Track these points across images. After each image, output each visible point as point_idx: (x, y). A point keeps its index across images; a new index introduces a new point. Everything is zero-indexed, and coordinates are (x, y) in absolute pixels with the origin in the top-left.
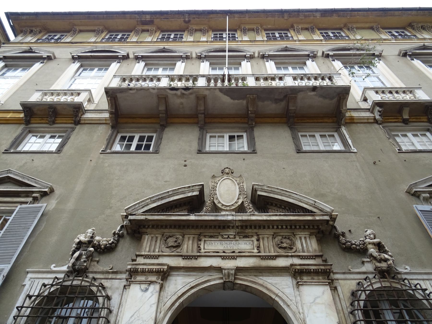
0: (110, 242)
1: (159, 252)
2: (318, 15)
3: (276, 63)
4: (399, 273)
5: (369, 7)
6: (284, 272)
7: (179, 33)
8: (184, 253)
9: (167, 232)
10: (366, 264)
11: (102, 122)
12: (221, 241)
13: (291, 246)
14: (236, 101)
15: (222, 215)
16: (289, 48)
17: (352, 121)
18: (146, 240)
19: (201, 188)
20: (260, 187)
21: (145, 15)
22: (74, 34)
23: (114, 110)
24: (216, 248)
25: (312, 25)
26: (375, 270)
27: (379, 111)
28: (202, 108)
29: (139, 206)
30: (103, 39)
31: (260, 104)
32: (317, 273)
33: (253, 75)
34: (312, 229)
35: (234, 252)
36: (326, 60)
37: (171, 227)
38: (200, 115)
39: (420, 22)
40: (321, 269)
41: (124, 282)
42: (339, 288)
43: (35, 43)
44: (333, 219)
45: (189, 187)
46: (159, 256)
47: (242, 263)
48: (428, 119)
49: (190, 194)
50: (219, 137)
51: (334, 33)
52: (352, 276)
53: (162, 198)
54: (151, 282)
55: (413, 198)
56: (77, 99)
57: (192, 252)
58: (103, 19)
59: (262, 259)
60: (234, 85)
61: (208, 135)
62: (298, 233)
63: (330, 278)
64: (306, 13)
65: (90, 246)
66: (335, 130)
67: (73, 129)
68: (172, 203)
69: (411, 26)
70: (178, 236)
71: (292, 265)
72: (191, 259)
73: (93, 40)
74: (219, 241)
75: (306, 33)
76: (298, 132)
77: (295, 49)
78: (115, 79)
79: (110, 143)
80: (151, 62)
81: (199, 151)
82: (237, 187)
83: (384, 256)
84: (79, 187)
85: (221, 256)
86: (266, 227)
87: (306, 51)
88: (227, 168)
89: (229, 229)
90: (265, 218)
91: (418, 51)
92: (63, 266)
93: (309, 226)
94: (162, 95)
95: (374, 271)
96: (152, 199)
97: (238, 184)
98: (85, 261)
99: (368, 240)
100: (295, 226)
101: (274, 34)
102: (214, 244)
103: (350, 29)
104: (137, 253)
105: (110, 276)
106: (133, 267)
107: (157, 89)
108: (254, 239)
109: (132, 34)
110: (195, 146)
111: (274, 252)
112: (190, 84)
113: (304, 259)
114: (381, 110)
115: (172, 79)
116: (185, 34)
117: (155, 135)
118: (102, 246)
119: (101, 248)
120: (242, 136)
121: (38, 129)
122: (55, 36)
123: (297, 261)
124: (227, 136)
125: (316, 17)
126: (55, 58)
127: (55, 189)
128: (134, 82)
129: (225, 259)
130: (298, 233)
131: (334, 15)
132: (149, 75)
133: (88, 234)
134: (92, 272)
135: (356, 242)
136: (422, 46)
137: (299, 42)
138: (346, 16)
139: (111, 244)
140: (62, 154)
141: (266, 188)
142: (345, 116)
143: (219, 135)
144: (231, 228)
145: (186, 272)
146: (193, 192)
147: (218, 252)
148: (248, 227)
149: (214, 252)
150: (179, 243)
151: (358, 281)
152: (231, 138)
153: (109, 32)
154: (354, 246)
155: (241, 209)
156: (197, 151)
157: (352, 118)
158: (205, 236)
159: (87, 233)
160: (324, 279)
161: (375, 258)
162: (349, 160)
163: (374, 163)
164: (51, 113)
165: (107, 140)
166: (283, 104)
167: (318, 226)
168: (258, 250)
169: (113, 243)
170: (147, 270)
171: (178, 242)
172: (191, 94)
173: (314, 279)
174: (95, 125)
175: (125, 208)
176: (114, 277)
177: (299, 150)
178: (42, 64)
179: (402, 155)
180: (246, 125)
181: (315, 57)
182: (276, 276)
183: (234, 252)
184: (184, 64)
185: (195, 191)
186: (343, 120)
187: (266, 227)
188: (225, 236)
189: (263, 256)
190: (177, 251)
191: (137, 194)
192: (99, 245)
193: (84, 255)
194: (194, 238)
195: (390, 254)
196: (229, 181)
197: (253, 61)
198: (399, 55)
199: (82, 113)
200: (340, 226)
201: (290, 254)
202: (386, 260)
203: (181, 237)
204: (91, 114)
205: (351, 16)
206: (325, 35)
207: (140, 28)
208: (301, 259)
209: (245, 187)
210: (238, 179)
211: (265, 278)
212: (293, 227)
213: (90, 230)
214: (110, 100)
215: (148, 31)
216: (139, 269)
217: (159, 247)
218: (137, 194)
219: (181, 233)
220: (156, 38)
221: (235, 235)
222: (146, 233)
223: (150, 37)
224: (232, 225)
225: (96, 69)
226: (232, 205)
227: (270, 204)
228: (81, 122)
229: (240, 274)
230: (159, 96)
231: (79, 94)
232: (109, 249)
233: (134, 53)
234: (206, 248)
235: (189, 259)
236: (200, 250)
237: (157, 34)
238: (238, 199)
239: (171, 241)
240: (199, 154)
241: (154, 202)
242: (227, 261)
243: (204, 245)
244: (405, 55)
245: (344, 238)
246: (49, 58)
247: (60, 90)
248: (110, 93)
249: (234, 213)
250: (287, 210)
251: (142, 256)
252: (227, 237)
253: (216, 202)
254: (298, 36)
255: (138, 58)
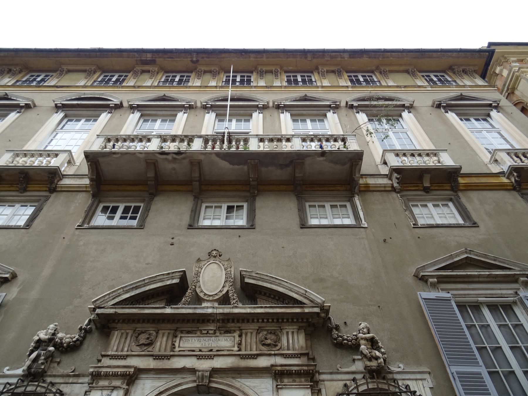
0: (74, 339)
1: (127, 351)
2: (346, 56)
3: (291, 115)
4: (391, 373)
5: (404, 48)
6: (265, 373)
7: (186, 74)
8: (156, 352)
9: (139, 327)
10: (356, 362)
11: (81, 189)
12: (199, 337)
13: (275, 342)
14: (236, 167)
15: (204, 308)
16: (308, 97)
17: (367, 189)
18: (115, 337)
19: (182, 275)
20: (248, 274)
21: (145, 54)
22: (61, 75)
23: (95, 177)
24: (193, 346)
25: (339, 67)
26: (365, 369)
27: (397, 178)
28: (197, 175)
29: (109, 298)
30: (95, 81)
31: (263, 169)
32: (299, 374)
33: (257, 135)
34: (302, 322)
35: (211, 350)
36: (350, 111)
37: (144, 321)
38: (194, 183)
39: (462, 65)
40: (304, 370)
41: (86, 387)
42: (323, 391)
43: (13, 86)
44: (325, 310)
45: (169, 274)
46: (127, 356)
47: (219, 363)
48: (452, 187)
49: (169, 282)
50: (216, 207)
51: (365, 76)
52: (339, 377)
53: (137, 288)
54: (115, 388)
55: (421, 283)
56: (54, 162)
57: (165, 351)
58: (96, 57)
59: (241, 358)
60: (233, 149)
61: (204, 205)
62: (285, 327)
63: (315, 379)
64: (332, 54)
65: (51, 344)
66: (348, 199)
67: (47, 198)
68: (148, 292)
69: (451, 69)
70: (151, 332)
71: (272, 366)
72: (163, 359)
73: (82, 83)
74: (197, 337)
75: (332, 76)
76: (306, 201)
77: (315, 98)
78: (99, 139)
79: (89, 215)
80: (148, 112)
81: (190, 225)
82: (224, 272)
83: (375, 353)
84: (46, 272)
85: (196, 356)
86: (251, 321)
87: (328, 100)
88: (215, 250)
89: (210, 323)
90: (248, 311)
91: (453, 102)
92: (18, 368)
93: (297, 320)
94: (151, 160)
95: (364, 370)
96: (125, 289)
97: (225, 269)
98: (42, 364)
99: (361, 335)
100: (283, 320)
101: (296, 76)
102: (191, 340)
103: (383, 72)
104: (103, 353)
105: (71, 380)
106: (96, 370)
107: (145, 153)
108: (236, 334)
109: (130, 75)
110: (186, 219)
111: (256, 350)
112: (184, 146)
113: (288, 357)
114: (399, 176)
115: (164, 139)
116: (193, 75)
117: (142, 205)
118: (65, 345)
119: (63, 347)
120: (243, 206)
121: (5, 198)
122: (38, 76)
123: (280, 361)
124: (225, 207)
125: (344, 58)
126: (35, 106)
127: (18, 273)
128: (119, 143)
129: (201, 359)
130: (285, 327)
131: (365, 56)
132: (138, 135)
133: (50, 331)
134: (50, 376)
135: (348, 337)
136: (458, 96)
137: (322, 88)
138: (378, 58)
139: (75, 342)
140: (31, 230)
141: (254, 275)
142: (358, 184)
143: (216, 205)
144: (211, 322)
145: (157, 374)
146: (173, 279)
147: (194, 351)
148: (231, 321)
149: (189, 351)
150: (151, 340)
151: (344, 382)
152: (230, 209)
153: (104, 72)
154: (345, 341)
155: (225, 300)
156: (187, 226)
157: (367, 186)
158: (182, 332)
159: (49, 329)
160: (306, 381)
161: (365, 356)
162: (357, 237)
163: (385, 241)
164: (21, 179)
165: (85, 213)
166: (289, 169)
167: (307, 319)
168: (238, 347)
169: (77, 340)
170: (111, 373)
171: (150, 339)
172: (184, 158)
173: (294, 381)
174: (74, 193)
175: (93, 300)
176: (75, 381)
177: (303, 225)
178: (18, 114)
179: (417, 230)
180: (248, 194)
181: (338, 108)
182: (257, 377)
183: (211, 350)
184: (186, 115)
185: (175, 278)
186: (356, 188)
187: (251, 321)
188: (204, 332)
189: (243, 355)
190: (148, 350)
191: (113, 280)
192: (61, 343)
193: (43, 355)
194: (169, 333)
195: (383, 350)
196: (215, 266)
197: (266, 112)
198: (433, 106)
199: (58, 179)
200: (335, 319)
201: (273, 352)
202: (377, 358)
203: (154, 333)
204: (70, 180)
205: (384, 58)
206: (354, 78)
207: (139, 68)
208: (285, 358)
209: (232, 273)
210: (226, 263)
211: (243, 381)
212: (280, 321)
213: (52, 326)
214: (91, 165)
215: (148, 71)
216: (102, 373)
217: (129, 346)
218: (113, 280)
219: (155, 328)
220: (158, 81)
221: (215, 331)
222: (115, 329)
223: (150, 80)
224: (212, 318)
225: (83, 121)
226: (216, 294)
227: (258, 292)
228: (58, 189)
229: (216, 376)
230: (148, 161)
231: (57, 155)
232: (73, 348)
233: (128, 102)
234: (181, 345)
235: (160, 359)
236: (175, 348)
237: (159, 76)
238: (223, 287)
239: (143, 339)
240: (189, 230)
241: (127, 292)
242: (202, 361)
243: (179, 343)
244: (439, 106)
245: (337, 332)
246: (28, 107)
247: (35, 151)
248: (91, 158)
249: (216, 305)
250: (277, 300)
251: (108, 356)
252: (206, 332)
253: (198, 290)
254: (322, 80)
255: (133, 108)
